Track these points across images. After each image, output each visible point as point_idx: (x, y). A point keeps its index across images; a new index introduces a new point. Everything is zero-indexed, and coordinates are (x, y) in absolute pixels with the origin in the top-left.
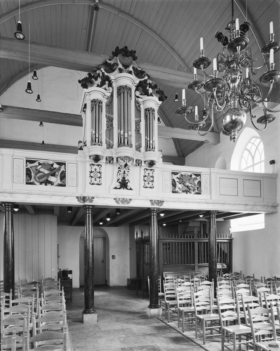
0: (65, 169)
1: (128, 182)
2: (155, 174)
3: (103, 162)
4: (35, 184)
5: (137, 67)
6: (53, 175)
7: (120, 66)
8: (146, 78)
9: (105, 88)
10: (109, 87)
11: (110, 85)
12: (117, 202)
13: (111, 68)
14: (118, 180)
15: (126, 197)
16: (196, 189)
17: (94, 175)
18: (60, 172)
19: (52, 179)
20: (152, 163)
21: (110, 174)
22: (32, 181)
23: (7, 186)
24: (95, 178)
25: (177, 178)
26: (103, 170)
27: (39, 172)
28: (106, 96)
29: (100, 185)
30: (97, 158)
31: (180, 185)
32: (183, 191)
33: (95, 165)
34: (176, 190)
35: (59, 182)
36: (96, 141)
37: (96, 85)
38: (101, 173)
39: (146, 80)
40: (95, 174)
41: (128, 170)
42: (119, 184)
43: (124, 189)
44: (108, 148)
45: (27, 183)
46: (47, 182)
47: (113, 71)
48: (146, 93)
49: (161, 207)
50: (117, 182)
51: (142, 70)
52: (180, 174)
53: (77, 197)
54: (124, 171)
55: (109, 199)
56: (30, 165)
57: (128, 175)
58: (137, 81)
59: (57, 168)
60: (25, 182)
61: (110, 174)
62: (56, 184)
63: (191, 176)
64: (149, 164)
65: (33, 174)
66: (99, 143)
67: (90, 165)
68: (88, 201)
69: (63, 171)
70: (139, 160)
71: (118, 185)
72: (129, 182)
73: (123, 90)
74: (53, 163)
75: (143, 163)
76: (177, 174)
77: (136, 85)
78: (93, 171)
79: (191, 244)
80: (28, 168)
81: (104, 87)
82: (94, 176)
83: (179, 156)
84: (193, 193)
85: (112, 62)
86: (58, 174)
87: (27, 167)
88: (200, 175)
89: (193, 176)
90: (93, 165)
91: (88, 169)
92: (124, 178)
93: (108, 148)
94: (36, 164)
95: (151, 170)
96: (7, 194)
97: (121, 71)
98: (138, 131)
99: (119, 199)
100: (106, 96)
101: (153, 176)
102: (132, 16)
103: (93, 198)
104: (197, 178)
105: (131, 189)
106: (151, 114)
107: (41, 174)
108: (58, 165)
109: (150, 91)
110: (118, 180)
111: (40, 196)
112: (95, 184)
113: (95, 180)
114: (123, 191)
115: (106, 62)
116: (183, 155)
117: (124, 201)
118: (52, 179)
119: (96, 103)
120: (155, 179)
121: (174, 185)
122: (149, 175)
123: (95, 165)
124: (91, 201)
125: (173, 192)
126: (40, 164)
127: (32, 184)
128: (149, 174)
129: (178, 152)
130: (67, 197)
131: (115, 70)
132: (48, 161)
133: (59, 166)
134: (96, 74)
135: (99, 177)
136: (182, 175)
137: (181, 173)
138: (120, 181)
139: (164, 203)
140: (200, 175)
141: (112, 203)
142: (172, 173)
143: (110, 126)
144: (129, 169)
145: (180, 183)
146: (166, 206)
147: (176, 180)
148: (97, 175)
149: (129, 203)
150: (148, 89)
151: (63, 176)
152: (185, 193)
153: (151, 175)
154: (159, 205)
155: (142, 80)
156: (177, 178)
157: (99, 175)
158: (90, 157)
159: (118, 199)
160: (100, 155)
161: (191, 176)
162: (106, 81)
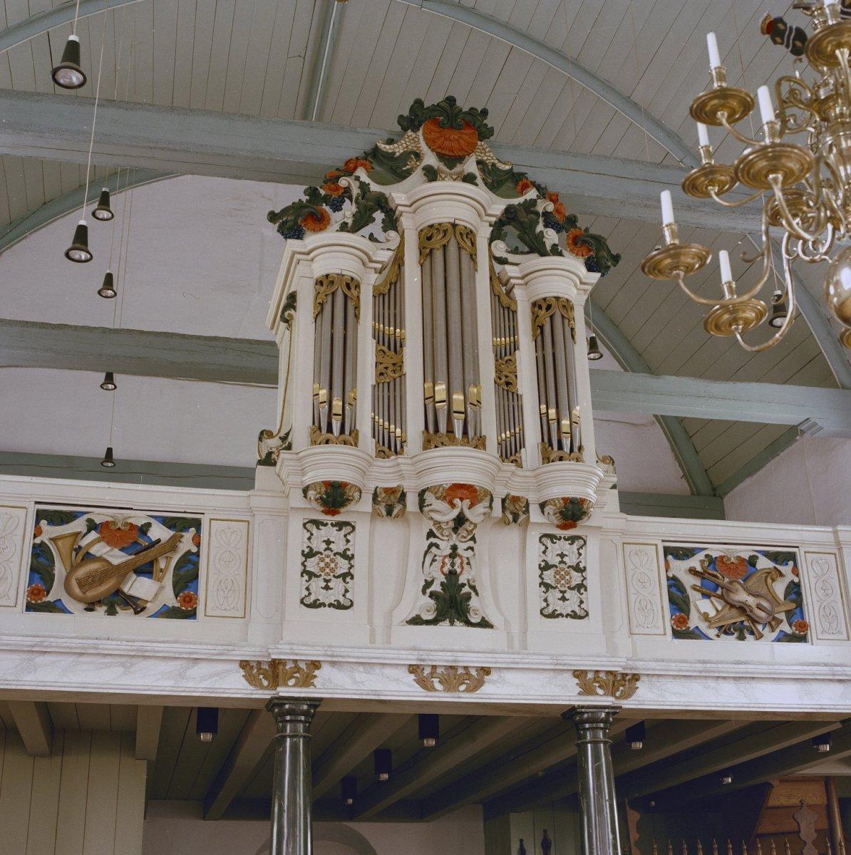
0: (198, 545)
1: (473, 594)
2: (592, 556)
4: (64, 610)
5: (496, 162)
6: (146, 570)
7: (430, 159)
8: (532, 194)
12: (424, 683)
14: (428, 584)
16: (782, 616)
19: (140, 587)
22: (51, 598)
25: (693, 571)
26: (360, 542)
27: (88, 557)
30: (334, 497)
31: (707, 601)
32: (725, 630)
36: (332, 426)
37: (337, 227)
39: (533, 203)
40: (327, 560)
41: (471, 544)
42: (432, 602)
43: (452, 623)
46: (118, 601)
47: (401, 175)
48: (537, 247)
50: (424, 592)
51: (516, 170)
52: (701, 556)
53: (244, 664)
54: (454, 548)
56: (49, 531)
58: (498, 206)
60: (22, 602)
61: (391, 561)
62: (152, 608)
63: (752, 561)
65: (59, 570)
70: (516, 499)
71: (426, 606)
72: (477, 594)
73: (442, 241)
75: (534, 510)
77: (493, 219)
80: (42, 543)
85: (398, 149)
86: (168, 565)
87: (38, 541)
89: (764, 563)
90: (317, 524)
91: (297, 540)
92: (452, 575)
93: (381, 454)
94: (78, 525)
95: (573, 539)
97: (431, 175)
99: (434, 667)
101: (581, 566)
103: (316, 665)
105: (484, 624)
108: (170, 528)
111: (83, 659)
112: (323, 605)
113: (327, 588)
117: (454, 676)
118: (140, 587)
120: (593, 579)
121: (679, 601)
122: (565, 563)
124: (307, 681)
126: (92, 526)
133: (172, 533)
134: (338, 188)
135: (344, 576)
138: (436, 587)
139: (638, 684)
143: (390, 373)
144: (473, 539)
147: (689, 581)
148: (332, 565)
149: (479, 684)
151: (187, 576)
154: (618, 694)
156: (693, 571)
159: (427, 671)
161: (752, 561)
162: (373, 208)
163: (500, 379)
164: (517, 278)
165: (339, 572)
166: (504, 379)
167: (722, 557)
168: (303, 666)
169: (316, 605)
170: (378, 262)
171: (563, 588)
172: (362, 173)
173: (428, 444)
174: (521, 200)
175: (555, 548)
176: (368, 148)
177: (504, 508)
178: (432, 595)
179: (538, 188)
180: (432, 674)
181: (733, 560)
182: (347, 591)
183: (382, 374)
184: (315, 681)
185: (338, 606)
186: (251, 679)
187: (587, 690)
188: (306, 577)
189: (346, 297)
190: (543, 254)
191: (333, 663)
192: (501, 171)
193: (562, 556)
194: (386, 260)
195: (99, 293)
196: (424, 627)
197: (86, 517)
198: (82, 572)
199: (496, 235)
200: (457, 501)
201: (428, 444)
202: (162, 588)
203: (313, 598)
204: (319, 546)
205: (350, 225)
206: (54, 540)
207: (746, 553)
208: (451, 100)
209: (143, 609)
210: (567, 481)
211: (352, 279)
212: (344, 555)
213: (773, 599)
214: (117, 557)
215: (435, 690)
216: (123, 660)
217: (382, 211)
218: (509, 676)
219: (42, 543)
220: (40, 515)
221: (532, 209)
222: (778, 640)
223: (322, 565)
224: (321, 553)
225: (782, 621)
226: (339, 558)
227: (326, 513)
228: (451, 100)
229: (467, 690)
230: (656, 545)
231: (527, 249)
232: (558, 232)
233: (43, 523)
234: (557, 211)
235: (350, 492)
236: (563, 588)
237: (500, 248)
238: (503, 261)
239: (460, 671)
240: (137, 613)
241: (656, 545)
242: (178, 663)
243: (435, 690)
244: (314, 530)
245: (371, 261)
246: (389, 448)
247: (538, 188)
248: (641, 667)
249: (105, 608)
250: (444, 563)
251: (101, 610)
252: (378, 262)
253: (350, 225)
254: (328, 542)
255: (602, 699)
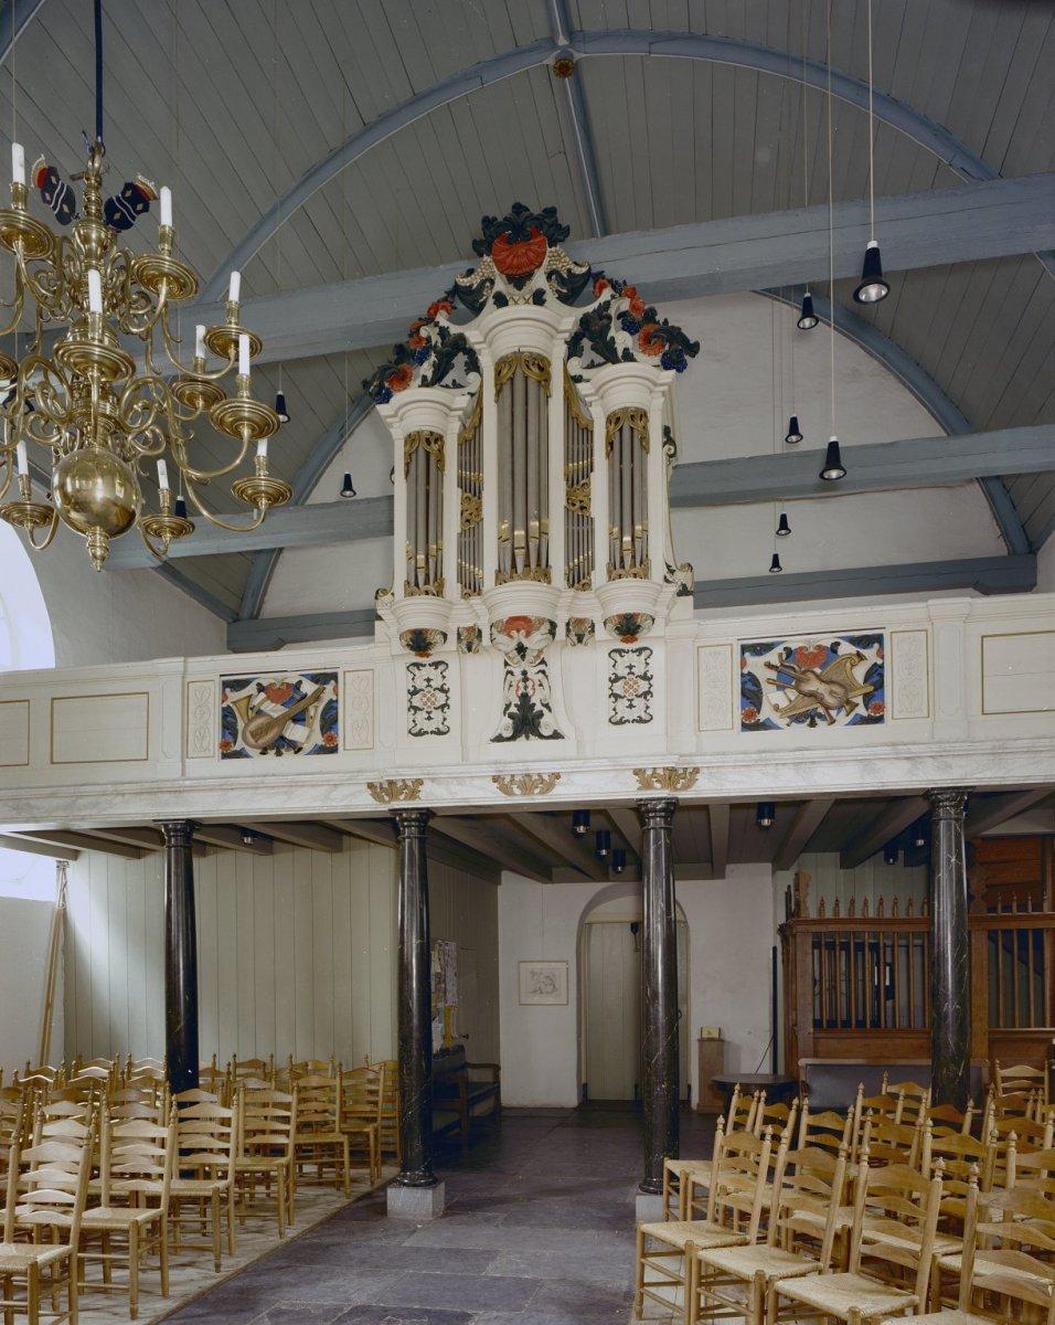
0: (882, 657)
1: (545, 711)
2: (657, 665)
3: (446, 650)
4: (247, 756)
5: (572, 266)
6: (299, 718)
7: (501, 285)
8: (606, 294)
9: (454, 381)
10: (467, 372)
11: (473, 365)
12: (506, 790)
13: (468, 301)
14: (508, 706)
15: (534, 769)
16: (859, 700)
17: (425, 699)
18: (321, 706)
19: (295, 732)
20: (628, 627)
21: (480, 686)
22: (237, 748)
23: (167, 767)
24: (428, 711)
25: (769, 666)
26: (452, 679)
27: (260, 713)
28: (456, 410)
29: (445, 733)
30: (419, 642)
31: (781, 693)
32: (797, 719)
33: (424, 666)
34: (762, 717)
35: (318, 739)
36: (427, 580)
37: (419, 381)
38: (446, 692)
39: (607, 304)
40: (429, 695)
41: (542, 667)
42: (511, 721)
43: (527, 738)
44: (466, 596)
45: (225, 756)
46: (281, 745)
47: (477, 309)
48: (609, 354)
49: (682, 795)
50: (505, 713)
51: (594, 271)
52: (779, 649)
53: (371, 786)
54: (524, 673)
55: (476, 782)
56: (233, 696)
57: (541, 685)
58: (569, 319)
59: (309, 694)
60: (218, 752)
61: (480, 686)
62: (308, 747)
63: (834, 647)
64: (617, 628)
65: (240, 725)
66: (638, 569)
67: (610, 654)
68: (402, 797)
69: (331, 701)
70: (580, 621)
71: (505, 725)
72: (550, 711)
73: (521, 375)
74: (836, 640)
75: (599, 627)
76: (768, 647)
77: (567, 336)
78: (620, 675)
79: (1027, 938)
80: (229, 706)
81: (448, 380)
82: (425, 704)
83: (1012, 552)
84: (842, 718)
85: (474, 281)
86: (315, 712)
87: (225, 705)
88: (879, 639)
89: (846, 649)
90: (417, 665)
91: (403, 681)
92: (525, 697)
93: (466, 596)
94: (251, 689)
95: (640, 651)
96: (167, 796)
97: (501, 301)
98: (582, 508)
99: (513, 776)
100: (456, 410)
101: (649, 675)
102: (704, 39)
103: (420, 782)
104: (862, 651)
105: (556, 735)
106: (626, 433)
107: (260, 721)
108: (316, 682)
109: (623, 340)
110: (508, 706)
111: (259, 791)
112: (426, 733)
113: (429, 718)
114: (528, 747)
115: (456, 286)
116: (1030, 544)
117: (528, 783)
118: (295, 732)
119: (425, 449)
120: (658, 686)
121: (751, 693)
122: (633, 674)
123: (424, 666)
124: (413, 794)
125: (746, 727)
126: (261, 688)
127: (766, 726)
128: (431, 683)
129: (1005, 535)
130: (340, 789)
131: (483, 305)
132: (283, 674)
133: (317, 686)
134: (421, 339)
135: (442, 707)
136: (789, 652)
137: (257, 681)
138: (513, 709)
139: (698, 776)
140: (879, 639)
141: (484, 795)
142: (226, 685)
143: (472, 520)
144: (543, 662)
145: (780, 688)
146: (706, 787)
147: (763, 675)
148: (433, 699)
149: (549, 787)
150: (613, 338)
151: (330, 721)
152: (803, 727)
153: (639, 670)
154: (679, 786)
155: (591, 310)
156: (769, 666)
157: (618, 688)
158: (605, 623)
159: (508, 779)
160: (427, 631)
161: (834, 647)
162: (455, 351)
163: (574, 505)
164: (592, 395)
165: (438, 704)
166: (578, 504)
167: (801, 648)
168: (410, 784)
169: (420, 733)
170: (662, 385)
171: (630, 696)
172: (442, 319)
173: (500, 578)
174: (595, 305)
175: (623, 662)
176: (450, 286)
177: (568, 630)
178: (511, 716)
179: (614, 285)
180: (512, 780)
181: (812, 650)
182: (445, 719)
183: (468, 521)
184: (420, 795)
185: (439, 732)
186: (377, 796)
187: (646, 785)
188: (413, 711)
189: (632, 429)
190: (615, 361)
191: (433, 780)
192: (578, 275)
193: (631, 667)
194: (464, 405)
195: (786, 440)
196: (506, 743)
197: (257, 681)
198: (253, 726)
199: (574, 348)
200: (514, 633)
201: (500, 578)
202: (311, 732)
203: (418, 728)
204: (420, 684)
205: (429, 379)
206: (234, 703)
207: (827, 641)
208: (518, 208)
209: (300, 749)
210: (627, 596)
211: (432, 433)
212: (442, 690)
213: (847, 687)
214: (274, 710)
215: (514, 794)
216: (285, 789)
217: (464, 354)
218: (576, 778)
219: (229, 706)
220: (226, 685)
221: (605, 313)
222: (854, 723)
223: (425, 699)
224: (423, 690)
225: (857, 705)
226: (639, 680)
227: (626, 641)
228: (518, 208)
229: (541, 793)
230: (731, 645)
231: (603, 360)
232: (632, 334)
233: (228, 690)
234: (633, 307)
235: (430, 638)
236: (630, 696)
237: (575, 366)
238: (578, 379)
239: (681, 771)
240: (296, 753)
241: (731, 645)
242: (324, 788)
243: (514, 794)
244: (416, 672)
245: (655, 384)
246: (475, 591)
247: (614, 285)
248: (698, 762)
249: (274, 751)
250: (518, 687)
251: (272, 753)
252: (662, 385)
253: (429, 379)
254: (428, 680)
255: (660, 792)
